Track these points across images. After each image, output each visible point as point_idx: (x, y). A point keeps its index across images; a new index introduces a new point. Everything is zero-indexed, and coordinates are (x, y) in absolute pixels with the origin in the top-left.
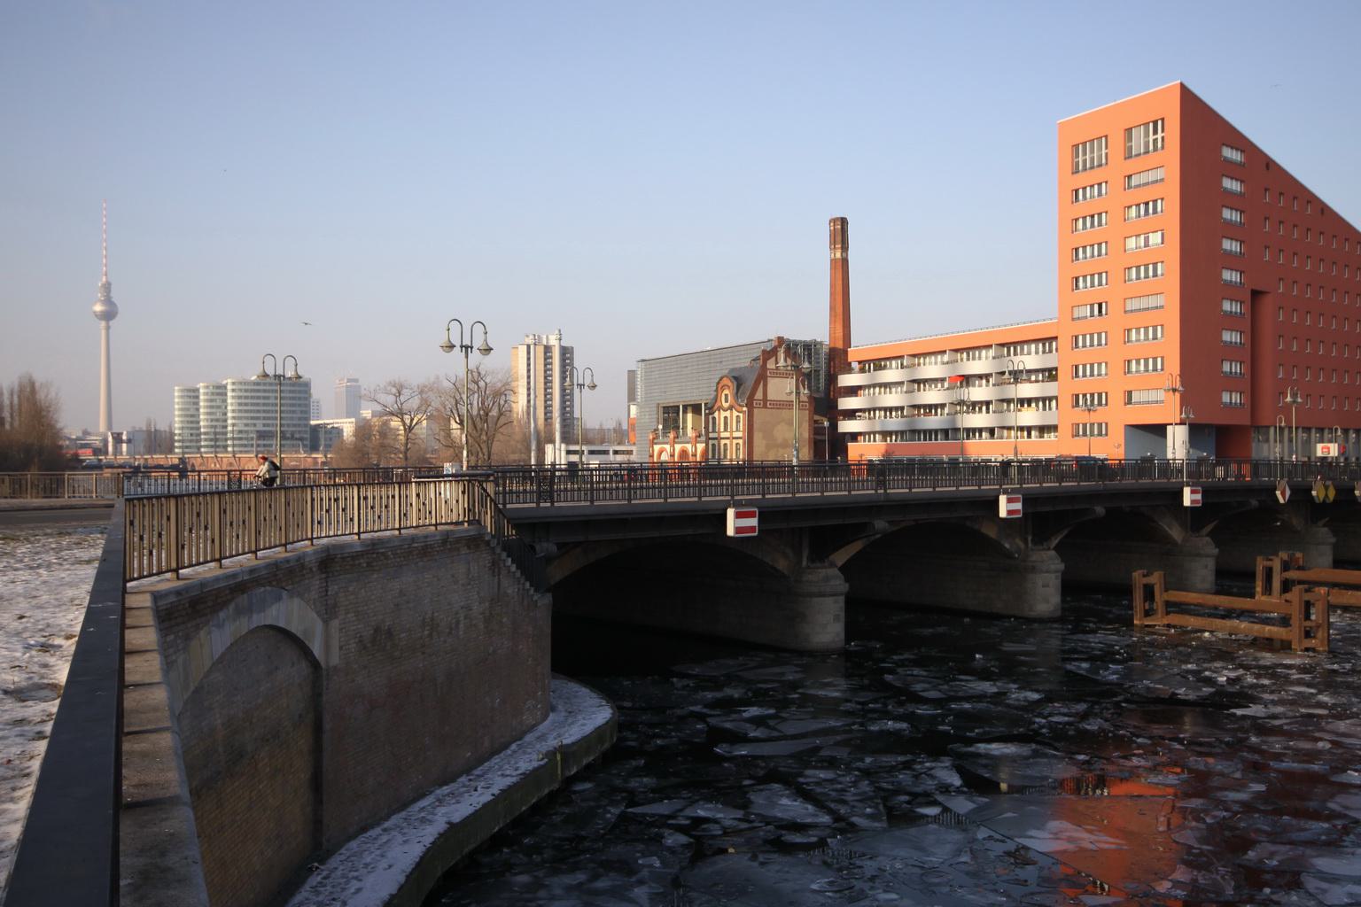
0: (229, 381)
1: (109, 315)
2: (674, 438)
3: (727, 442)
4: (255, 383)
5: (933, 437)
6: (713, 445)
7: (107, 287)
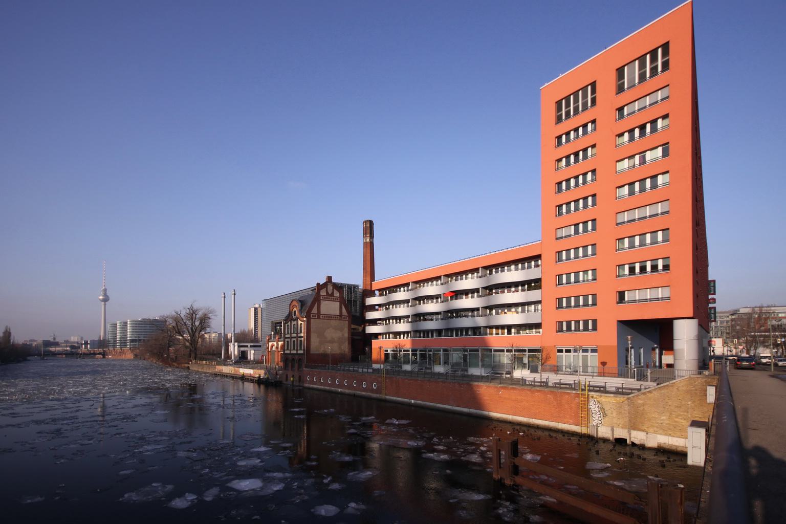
0: (129, 320)
1: (106, 300)
2: (278, 339)
3: (295, 339)
4: (140, 321)
5: (430, 335)
6: (288, 342)
7: (105, 290)
